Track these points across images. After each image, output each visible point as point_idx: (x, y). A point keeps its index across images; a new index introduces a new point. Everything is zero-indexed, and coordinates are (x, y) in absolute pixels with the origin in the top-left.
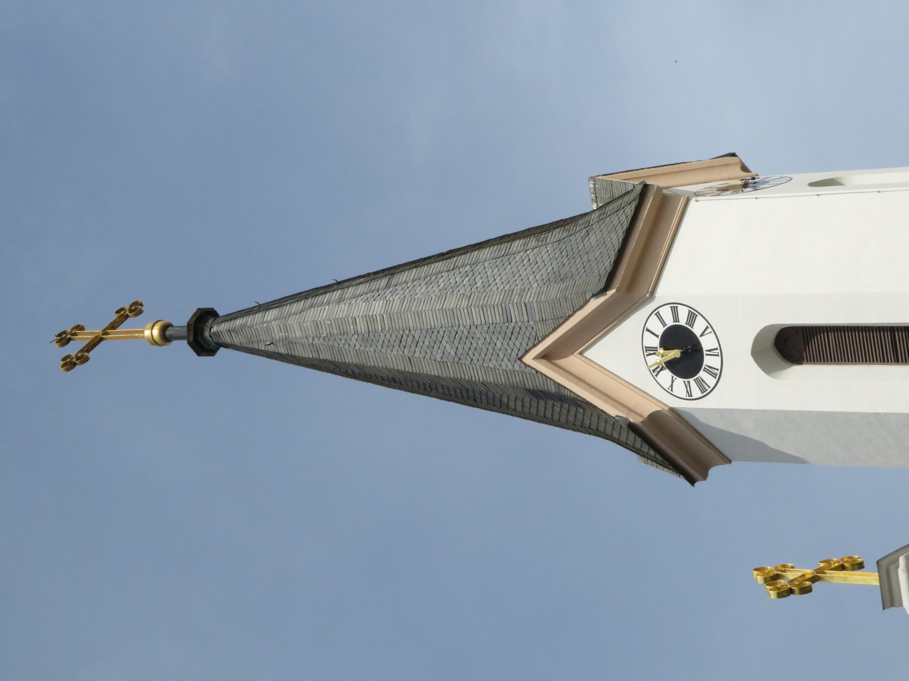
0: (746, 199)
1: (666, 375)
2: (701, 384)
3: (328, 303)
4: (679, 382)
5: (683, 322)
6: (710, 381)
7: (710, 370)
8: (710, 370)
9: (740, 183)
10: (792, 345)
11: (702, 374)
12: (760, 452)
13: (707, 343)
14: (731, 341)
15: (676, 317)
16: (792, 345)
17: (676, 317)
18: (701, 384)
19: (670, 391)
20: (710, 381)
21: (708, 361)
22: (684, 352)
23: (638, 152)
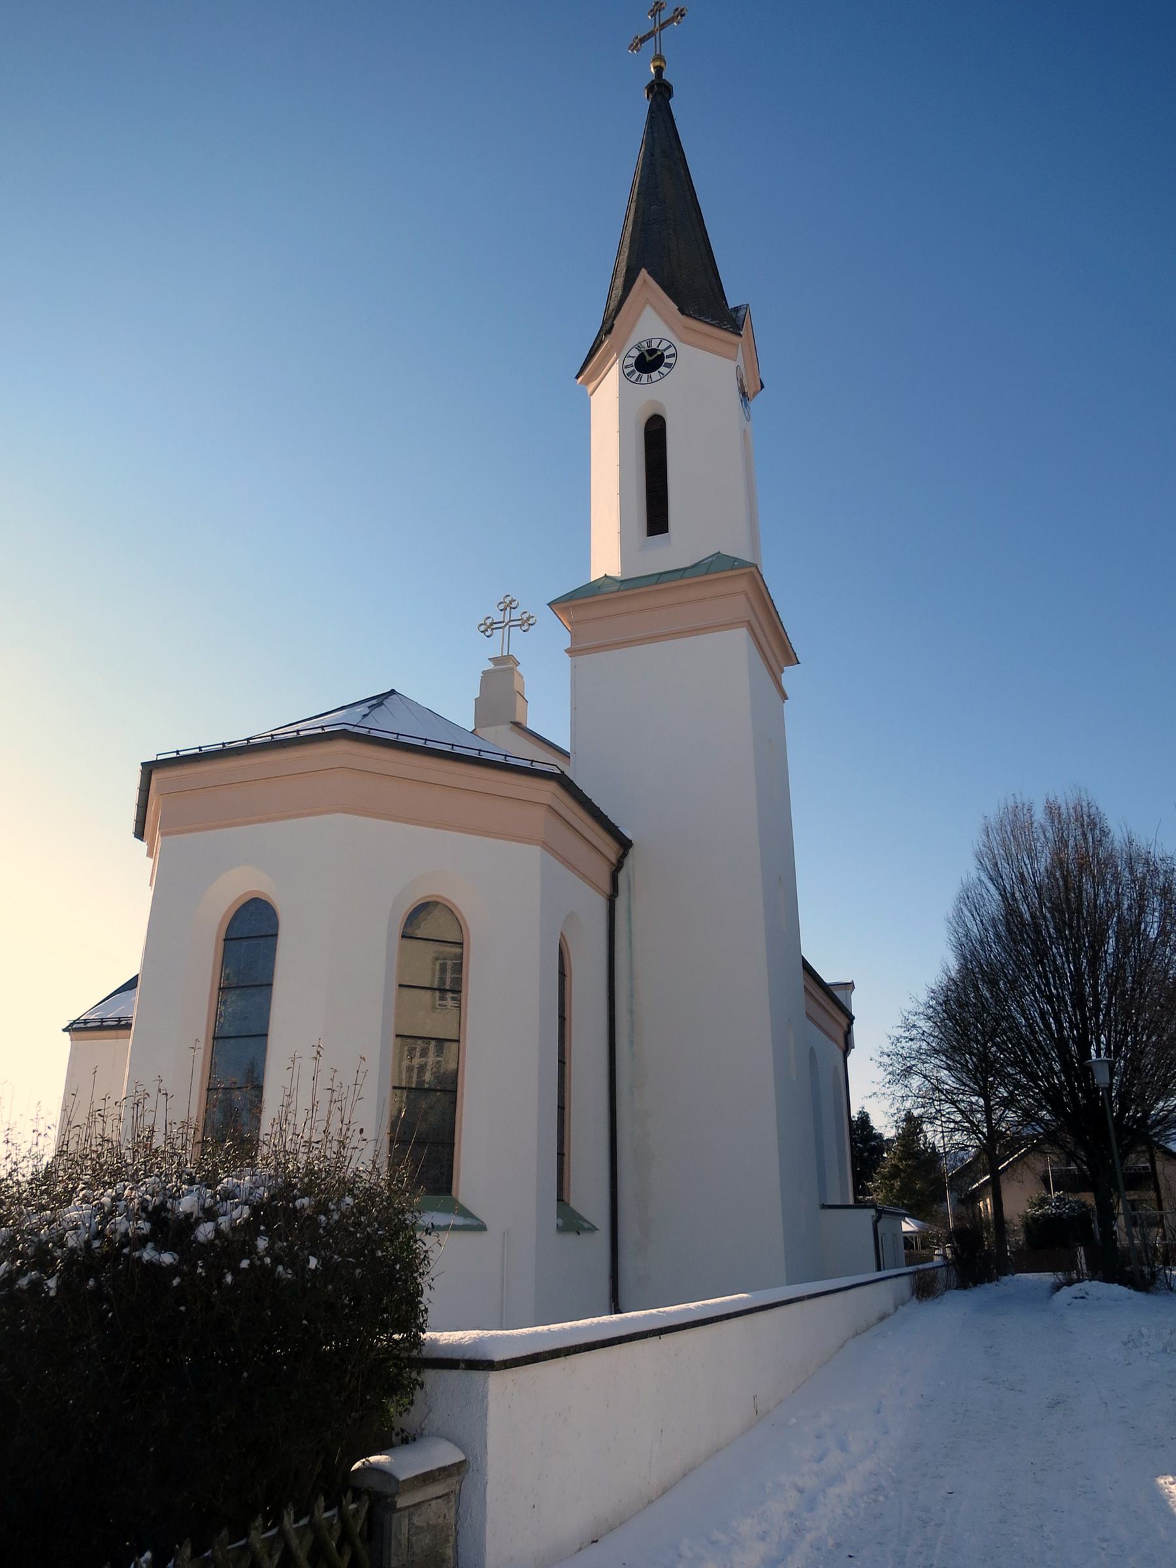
0: (737, 396)
1: (636, 353)
2: (632, 373)
3: (401, 1101)
4: (633, 361)
5: (666, 361)
6: (633, 378)
7: (639, 378)
8: (639, 378)
9: (746, 390)
10: (654, 435)
11: (637, 373)
12: (1050, 1298)
13: (655, 375)
14: (660, 391)
15: (668, 357)
16: (654, 435)
17: (668, 357)
18: (632, 373)
19: (628, 356)
20: (633, 378)
21: (645, 376)
22: (649, 362)
23: (758, 321)
